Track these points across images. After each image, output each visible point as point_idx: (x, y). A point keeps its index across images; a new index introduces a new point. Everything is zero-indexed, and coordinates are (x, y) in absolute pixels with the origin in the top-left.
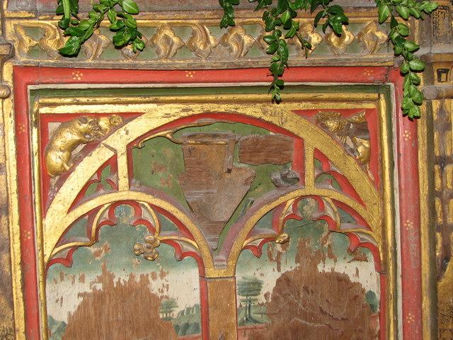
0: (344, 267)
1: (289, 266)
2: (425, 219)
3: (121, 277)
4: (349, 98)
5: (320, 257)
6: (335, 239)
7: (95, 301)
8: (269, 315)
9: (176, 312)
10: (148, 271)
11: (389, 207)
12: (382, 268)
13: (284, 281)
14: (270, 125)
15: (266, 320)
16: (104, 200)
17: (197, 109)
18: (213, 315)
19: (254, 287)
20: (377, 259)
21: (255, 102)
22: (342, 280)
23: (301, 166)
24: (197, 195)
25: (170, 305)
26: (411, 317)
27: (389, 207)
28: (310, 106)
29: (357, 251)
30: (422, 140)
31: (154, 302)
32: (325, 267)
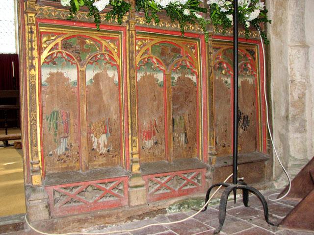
0: (190, 76)
1: (180, 75)
2: (207, 65)
3: (148, 73)
4: (271, 101)
5: (185, 74)
6: (188, 70)
7: (143, 78)
8: (176, 85)
9: (159, 82)
10: (154, 73)
11: (199, 64)
12: (197, 78)
13: (179, 78)
14: (177, 45)
15: (175, 86)
16: (146, 56)
17: (164, 40)
18: (167, 82)
19: (173, 79)
20: (196, 75)
21: (174, 40)
22: (189, 79)
23: (183, 54)
24: (163, 58)
25: (158, 80)
26: (205, 137)
27: (199, 64)
28: (101, 35)
29: (192, 74)
30: (206, 49)
31: (154, 79)
32: (186, 76)
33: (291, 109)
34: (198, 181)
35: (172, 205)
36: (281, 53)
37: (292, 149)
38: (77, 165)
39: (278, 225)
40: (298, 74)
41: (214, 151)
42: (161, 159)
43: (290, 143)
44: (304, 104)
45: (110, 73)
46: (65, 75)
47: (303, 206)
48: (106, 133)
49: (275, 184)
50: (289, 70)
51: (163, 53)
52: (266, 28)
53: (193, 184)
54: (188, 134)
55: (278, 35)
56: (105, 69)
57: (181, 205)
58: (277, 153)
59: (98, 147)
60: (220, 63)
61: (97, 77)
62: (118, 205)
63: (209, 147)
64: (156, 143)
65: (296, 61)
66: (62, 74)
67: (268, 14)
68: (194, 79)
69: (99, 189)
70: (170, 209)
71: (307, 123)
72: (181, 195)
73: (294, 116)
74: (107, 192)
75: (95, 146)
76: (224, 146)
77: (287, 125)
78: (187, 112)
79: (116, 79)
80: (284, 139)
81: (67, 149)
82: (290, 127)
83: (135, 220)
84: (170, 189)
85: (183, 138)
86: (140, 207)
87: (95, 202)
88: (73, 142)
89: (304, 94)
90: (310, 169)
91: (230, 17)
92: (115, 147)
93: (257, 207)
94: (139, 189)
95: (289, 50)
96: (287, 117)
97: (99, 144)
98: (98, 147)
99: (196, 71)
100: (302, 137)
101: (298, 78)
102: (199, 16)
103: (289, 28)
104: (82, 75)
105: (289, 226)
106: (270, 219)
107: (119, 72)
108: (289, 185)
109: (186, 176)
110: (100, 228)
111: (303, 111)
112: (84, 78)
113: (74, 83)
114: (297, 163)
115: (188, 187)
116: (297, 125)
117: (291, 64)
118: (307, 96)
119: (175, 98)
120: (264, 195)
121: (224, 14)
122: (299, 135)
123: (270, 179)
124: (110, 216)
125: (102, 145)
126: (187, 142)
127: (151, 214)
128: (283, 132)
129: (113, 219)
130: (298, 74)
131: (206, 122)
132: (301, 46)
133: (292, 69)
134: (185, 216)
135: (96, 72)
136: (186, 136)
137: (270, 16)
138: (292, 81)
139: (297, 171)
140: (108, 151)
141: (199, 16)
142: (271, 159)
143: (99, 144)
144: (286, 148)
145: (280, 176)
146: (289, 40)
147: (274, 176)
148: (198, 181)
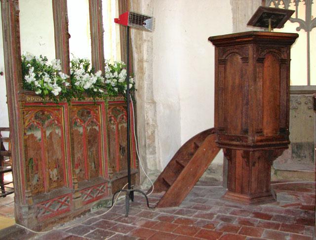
12: (99, 127)
32: (93, 127)
33: (147, 140)
34: (68, 202)
35: (94, 206)
36: (142, 107)
37: (148, 164)
38: (43, 189)
39: (155, 208)
40: (151, 120)
41: (111, 172)
42: (84, 179)
43: (147, 161)
44: (154, 137)
45: (57, 131)
46: (35, 135)
47: (167, 195)
48: (56, 168)
49: (142, 187)
50: (146, 117)
51: (82, 115)
52: (134, 94)
53: (103, 192)
54: (96, 163)
55: (140, 96)
56: (55, 129)
57: (98, 205)
58: (142, 168)
59: (53, 177)
60: (110, 117)
61: (51, 134)
62: (68, 210)
63: (108, 169)
64: (81, 170)
65: (150, 112)
66: (33, 135)
67: (135, 85)
68: (97, 128)
69: (59, 202)
70: (93, 208)
71: (156, 148)
72: (97, 200)
73: (149, 145)
74: (62, 203)
75: (51, 177)
76: (113, 167)
77: (145, 151)
78: (95, 149)
79: (60, 134)
80: (144, 159)
81: (38, 181)
82: (147, 151)
83: (77, 218)
84: (67, 205)
85: (93, 166)
86: (284, 147)
87: (57, 210)
88: (40, 175)
89: (154, 132)
90: (162, 176)
91: (116, 89)
92: (61, 174)
93: (139, 200)
94: (79, 199)
95: (146, 105)
96: (145, 145)
97: (53, 175)
98: (53, 177)
99: (99, 123)
100: (154, 157)
101: (151, 122)
102: (101, 91)
103: (145, 91)
104: (44, 132)
105: (160, 207)
106: (150, 206)
107: (62, 131)
108: (152, 187)
109: (44, 206)
110: (62, 225)
111: (154, 141)
112: (45, 135)
113: (40, 140)
114: (151, 172)
115: (100, 194)
116: (151, 150)
117: (92, 139)
118: (156, 132)
119: (89, 141)
120: (136, 196)
121: (113, 87)
122: (152, 156)
123: (139, 184)
124: (66, 217)
125: (55, 176)
126: (95, 168)
127: (84, 213)
128: (144, 155)
129: (68, 219)
130: (151, 120)
131: (106, 155)
132: (152, 103)
133: (147, 116)
134: (103, 212)
135: (50, 131)
136: (95, 164)
137: (136, 87)
138: (148, 124)
139: (155, 178)
140: (58, 179)
141: (101, 91)
142: (138, 173)
143: (53, 175)
144: (146, 164)
145: (144, 181)
146: (145, 99)
147: (141, 182)
148: (68, 202)
